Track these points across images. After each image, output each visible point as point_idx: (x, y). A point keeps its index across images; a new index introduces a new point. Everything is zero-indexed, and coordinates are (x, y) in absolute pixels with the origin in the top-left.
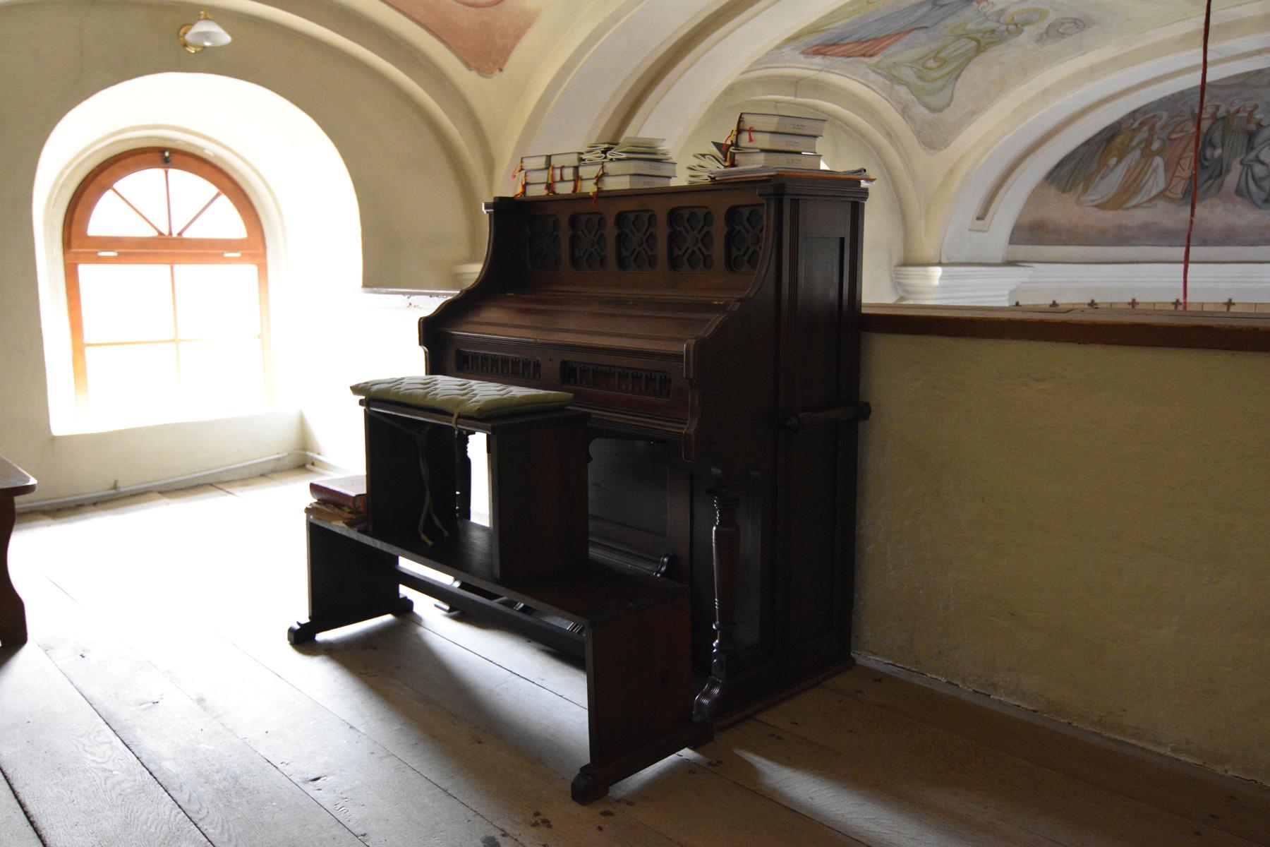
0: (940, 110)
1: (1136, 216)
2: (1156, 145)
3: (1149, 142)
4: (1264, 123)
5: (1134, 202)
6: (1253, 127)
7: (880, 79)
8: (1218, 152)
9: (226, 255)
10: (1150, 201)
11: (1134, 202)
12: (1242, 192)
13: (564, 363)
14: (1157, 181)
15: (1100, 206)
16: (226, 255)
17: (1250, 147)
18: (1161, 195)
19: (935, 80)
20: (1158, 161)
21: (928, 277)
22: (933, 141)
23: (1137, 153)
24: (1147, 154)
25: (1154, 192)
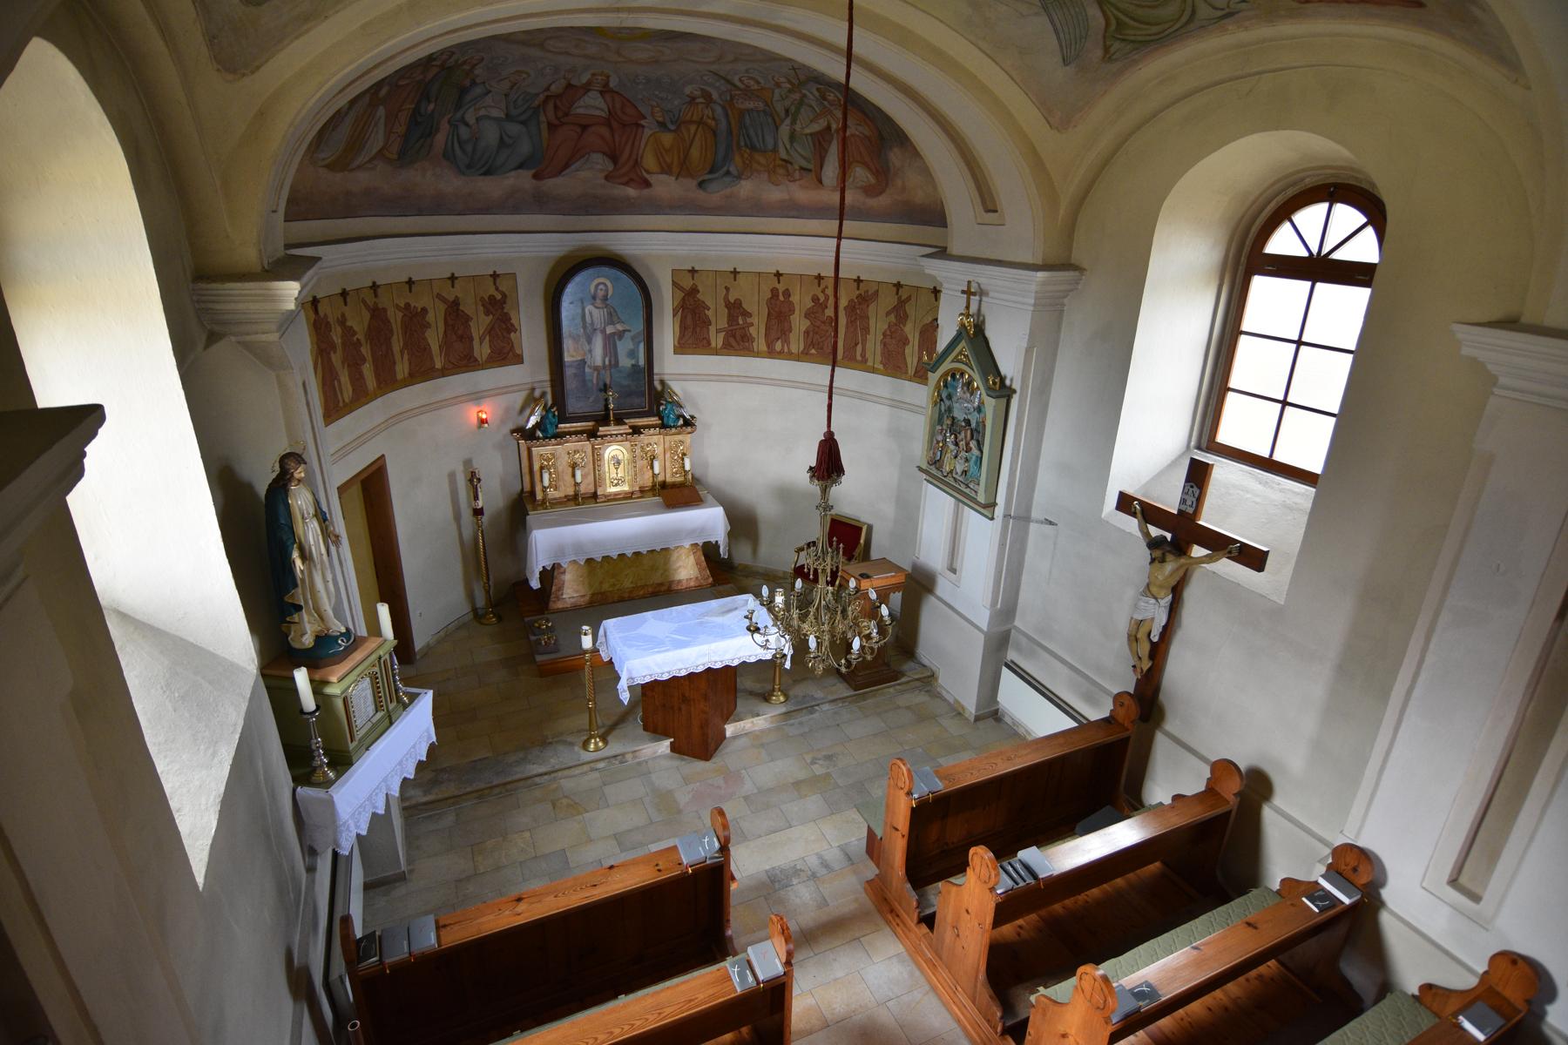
6: (467, 83)
8: (432, 106)
9: (1155, 867)
10: (370, 161)
11: (360, 160)
12: (448, 156)
13: (676, 352)
15: (330, 167)
16: (1155, 867)
17: (458, 106)
21: (272, 298)
25: (375, 151)
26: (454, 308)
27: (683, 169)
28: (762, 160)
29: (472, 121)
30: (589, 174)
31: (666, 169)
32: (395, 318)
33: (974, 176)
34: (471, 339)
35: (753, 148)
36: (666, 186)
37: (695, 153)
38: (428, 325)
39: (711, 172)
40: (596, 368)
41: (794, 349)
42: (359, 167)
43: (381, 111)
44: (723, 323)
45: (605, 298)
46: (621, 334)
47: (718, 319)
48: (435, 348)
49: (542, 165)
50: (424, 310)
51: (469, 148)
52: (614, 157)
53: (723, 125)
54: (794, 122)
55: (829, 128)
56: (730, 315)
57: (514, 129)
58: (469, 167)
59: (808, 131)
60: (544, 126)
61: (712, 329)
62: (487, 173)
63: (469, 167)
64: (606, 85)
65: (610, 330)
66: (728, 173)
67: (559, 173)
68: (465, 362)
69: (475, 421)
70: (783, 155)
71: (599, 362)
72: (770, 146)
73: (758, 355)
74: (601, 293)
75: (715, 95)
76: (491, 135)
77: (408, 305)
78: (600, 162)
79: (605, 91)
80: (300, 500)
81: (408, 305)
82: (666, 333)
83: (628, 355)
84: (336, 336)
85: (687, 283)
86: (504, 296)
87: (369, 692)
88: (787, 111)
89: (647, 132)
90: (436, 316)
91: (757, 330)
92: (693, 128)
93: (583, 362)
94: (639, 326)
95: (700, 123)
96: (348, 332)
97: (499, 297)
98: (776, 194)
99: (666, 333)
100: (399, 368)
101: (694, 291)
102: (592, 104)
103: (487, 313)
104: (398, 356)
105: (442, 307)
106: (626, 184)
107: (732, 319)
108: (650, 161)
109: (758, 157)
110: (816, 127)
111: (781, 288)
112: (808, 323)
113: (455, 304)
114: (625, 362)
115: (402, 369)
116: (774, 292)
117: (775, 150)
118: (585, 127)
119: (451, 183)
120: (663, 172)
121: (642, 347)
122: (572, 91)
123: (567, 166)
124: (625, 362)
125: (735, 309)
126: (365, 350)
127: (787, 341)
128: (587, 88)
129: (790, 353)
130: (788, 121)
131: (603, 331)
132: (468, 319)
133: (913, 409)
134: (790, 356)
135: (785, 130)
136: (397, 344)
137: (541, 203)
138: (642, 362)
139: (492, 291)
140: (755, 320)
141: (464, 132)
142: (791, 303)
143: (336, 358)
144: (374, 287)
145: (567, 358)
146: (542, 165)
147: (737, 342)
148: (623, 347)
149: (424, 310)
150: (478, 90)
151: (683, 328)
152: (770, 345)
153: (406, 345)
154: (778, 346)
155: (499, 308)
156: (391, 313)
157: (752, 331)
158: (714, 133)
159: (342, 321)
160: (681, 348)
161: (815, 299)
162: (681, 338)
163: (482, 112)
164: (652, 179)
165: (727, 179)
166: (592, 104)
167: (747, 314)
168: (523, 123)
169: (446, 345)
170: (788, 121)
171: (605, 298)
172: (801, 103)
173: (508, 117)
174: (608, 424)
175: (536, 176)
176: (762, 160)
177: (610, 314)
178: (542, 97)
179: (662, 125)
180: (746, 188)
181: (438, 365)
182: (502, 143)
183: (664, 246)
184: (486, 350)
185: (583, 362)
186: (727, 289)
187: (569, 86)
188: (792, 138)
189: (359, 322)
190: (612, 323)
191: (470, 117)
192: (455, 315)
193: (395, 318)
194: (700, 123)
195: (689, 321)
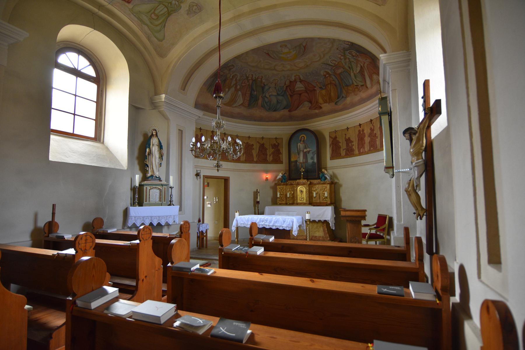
0: (162, 41)
1: (237, 110)
2: (238, 87)
3: (236, 85)
4: (266, 84)
5: (234, 106)
7: (136, 19)
8: (255, 93)
10: (239, 106)
12: (263, 106)
14: (240, 101)
17: (263, 93)
18: (242, 104)
19: (157, 26)
20: (240, 93)
21: (161, 98)
22: (162, 55)
23: (233, 89)
24: (236, 90)
25: (240, 103)
27: (329, 100)
28: (351, 89)
29: (268, 97)
30: (305, 108)
31: (325, 102)
33: (354, 30)
34: (267, 155)
35: (347, 86)
36: (326, 107)
37: (332, 94)
38: (254, 149)
39: (338, 98)
40: (301, 163)
41: (366, 150)
42: (235, 107)
43: (240, 93)
45: (304, 141)
46: (309, 152)
48: (255, 155)
49: (290, 107)
50: (253, 145)
52: (310, 102)
53: (337, 82)
54: (353, 71)
55: (361, 67)
56: (347, 143)
57: (280, 98)
59: (358, 72)
60: (289, 96)
61: (342, 149)
62: (275, 111)
63: (269, 109)
64: (300, 79)
65: (305, 150)
66: (343, 97)
68: (264, 161)
69: (265, 178)
70: (355, 84)
71: (301, 161)
72: (351, 83)
73: (356, 155)
75: (330, 72)
76: (274, 100)
77: (247, 143)
78: (307, 104)
79: (301, 81)
80: (154, 141)
81: (247, 143)
83: (312, 159)
85: (333, 136)
86: (279, 144)
87: (158, 194)
88: (349, 68)
89: (318, 91)
90: (256, 147)
91: (355, 147)
92: (329, 86)
93: (296, 161)
94: (314, 149)
95: (331, 83)
97: (277, 144)
98: (357, 98)
101: (336, 137)
102: (299, 86)
103: (273, 148)
105: (258, 145)
106: (315, 109)
107: (347, 145)
108: (321, 101)
109: (350, 88)
110: (359, 69)
111: (361, 129)
112: (369, 138)
113: (263, 144)
114: (310, 161)
116: (359, 131)
117: (353, 83)
118: (300, 94)
119: (264, 113)
120: (325, 103)
122: (292, 83)
124: (310, 161)
125: (348, 141)
127: (364, 148)
128: (295, 81)
129: (365, 152)
130: (351, 71)
131: (303, 151)
132: (266, 149)
134: (367, 153)
135: (352, 74)
137: (291, 118)
138: (315, 161)
139: (275, 142)
140: (354, 143)
141: (266, 99)
142: (364, 133)
145: (292, 160)
146: (290, 107)
147: (350, 153)
148: (309, 156)
149: (253, 145)
150: (267, 87)
151: (333, 151)
152: (359, 151)
155: (276, 147)
157: (354, 147)
158: (336, 85)
160: (332, 158)
161: (371, 129)
163: (270, 94)
164: (322, 106)
165: (343, 99)
166: (299, 86)
167: (352, 142)
168: (283, 96)
170: (351, 71)
171: (304, 141)
172: (350, 62)
173: (278, 95)
174: (300, 179)
175: (289, 111)
176: (351, 89)
177: (305, 146)
178: (285, 87)
179: (321, 88)
180: (348, 100)
181: (255, 160)
184: (271, 158)
185: (296, 161)
186: (346, 135)
187: (290, 82)
188: (355, 77)
190: (306, 148)
191: (267, 95)
192: (262, 148)
194: (331, 83)
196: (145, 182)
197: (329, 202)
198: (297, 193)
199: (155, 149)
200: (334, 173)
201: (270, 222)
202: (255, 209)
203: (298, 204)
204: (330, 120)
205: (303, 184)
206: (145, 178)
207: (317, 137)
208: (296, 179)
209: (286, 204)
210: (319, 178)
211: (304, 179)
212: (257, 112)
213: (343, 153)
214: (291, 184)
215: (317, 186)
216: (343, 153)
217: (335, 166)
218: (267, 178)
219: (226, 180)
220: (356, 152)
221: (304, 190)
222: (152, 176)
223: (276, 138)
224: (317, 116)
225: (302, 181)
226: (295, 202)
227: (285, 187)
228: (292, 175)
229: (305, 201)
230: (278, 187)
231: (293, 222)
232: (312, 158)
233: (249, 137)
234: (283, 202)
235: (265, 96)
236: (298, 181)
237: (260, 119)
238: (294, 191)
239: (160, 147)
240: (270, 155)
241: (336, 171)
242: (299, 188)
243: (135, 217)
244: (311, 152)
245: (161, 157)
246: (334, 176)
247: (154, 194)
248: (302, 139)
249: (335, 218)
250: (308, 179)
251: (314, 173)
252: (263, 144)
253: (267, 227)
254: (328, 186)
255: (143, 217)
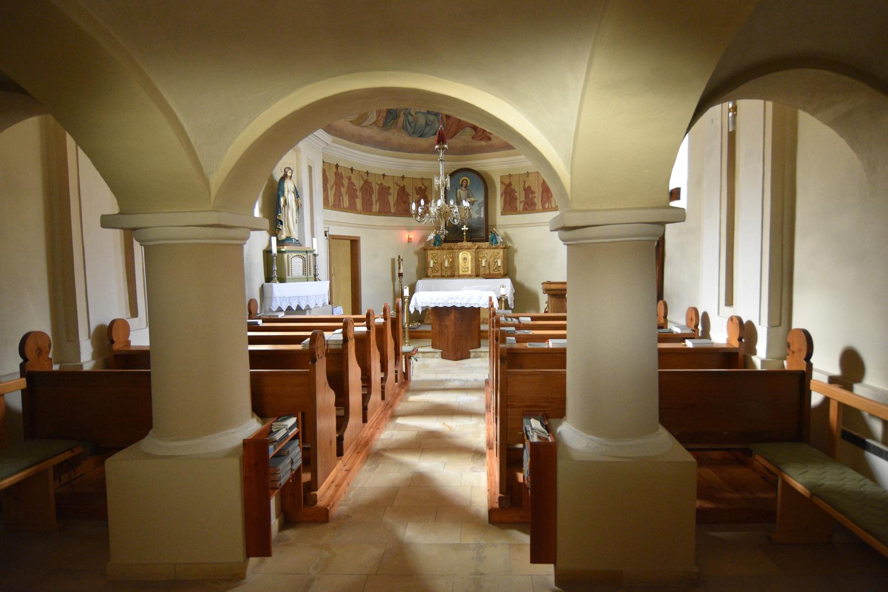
1: (367, 132)
12: (404, 128)
18: (375, 123)
25: (373, 121)
26: (402, 189)
32: (375, 188)
44: (523, 198)
45: (466, 186)
47: (521, 196)
48: (392, 203)
51: (413, 125)
58: (413, 133)
61: (518, 202)
62: (421, 136)
63: (413, 133)
67: (452, 137)
73: (538, 211)
74: (464, 184)
77: (381, 184)
80: (289, 185)
81: (381, 184)
82: (498, 203)
84: (345, 182)
85: (507, 182)
87: (301, 265)
91: (538, 200)
96: (351, 184)
99: (498, 203)
100: (374, 207)
101: (510, 184)
104: (374, 202)
107: (527, 196)
113: (403, 188)
115: (376, 207)
121: (483, 209)
123: (455, 134)
125: (528, 191)
126: (359, 194)
133: (819, 371)
136: (375, 197)
138: (482, 215)
139: (420, 185)
140: (536, 195)
141: (410, 118)
143: (344, 190)
144: (367, 173)
151: (505, 202)
152: (543, 206)
153: (379, 199)
154: (547, 206)
156: (374, 185)
157: (536, 200)
159: (349, 179)
160: (504, 212)
162: (505, 206)
167: (533, 192)
169: (397, 204)
171: (466, 186)
174: (462, 241)
181: (393, 211)
182: (427, 124)
183: (420, 350)
189: (358, 184)
192: (367, 188)
193: (375, 188)
195: (508, 199)
196: (285, 248)
197: (502, 271)
198: (458, 260)
199: (291, 198)
200: (506, 234)
201: (462, 299)
202: (394, 285)
203: (460, 277)
204: (503, 159)
205: (469, 249)
206: (280, 243)
207: (483, 180)
208: (457, 241)
209: (442, 277)
210: (487, 240)
211: (468, 241)
212: (396, 136)
213: (520, 207)
214: (449, 249)
215: (486, 251)
216: (520, 207)
217: (506, 224)
218: (409, 239)
219: (354, 243)
220: (539, 206)
221: (469, 257)
222: (288, 238)
223: (422, 179)
224: (482, 150)
225: (465, 244)
226: (456, 274)
227: (440, 252)
228: (454, 236)
229: (469, 273)
230: (429, 252)
231: (490, 299)
232: (478, 212)
233: (384, 175)
234: (437, 274)
235: (410, 113)
236: (459, 244)
237: (400, 148)
238: (453, 258)
239: (297, 194)
240: (332, 188)
241: (510, 231)
242: (461, 255)
243: (280, 298)
244: (476, 203)
245: (299, 207)
246: (506, 238)
247: (296, 265)
248: (464, 184)
249: (514, 294)
250: (473, 241)
251: (480, 233)
252: (403, 188)
253: (459, 306)
254: (501, 252)
255: (290, 298)
